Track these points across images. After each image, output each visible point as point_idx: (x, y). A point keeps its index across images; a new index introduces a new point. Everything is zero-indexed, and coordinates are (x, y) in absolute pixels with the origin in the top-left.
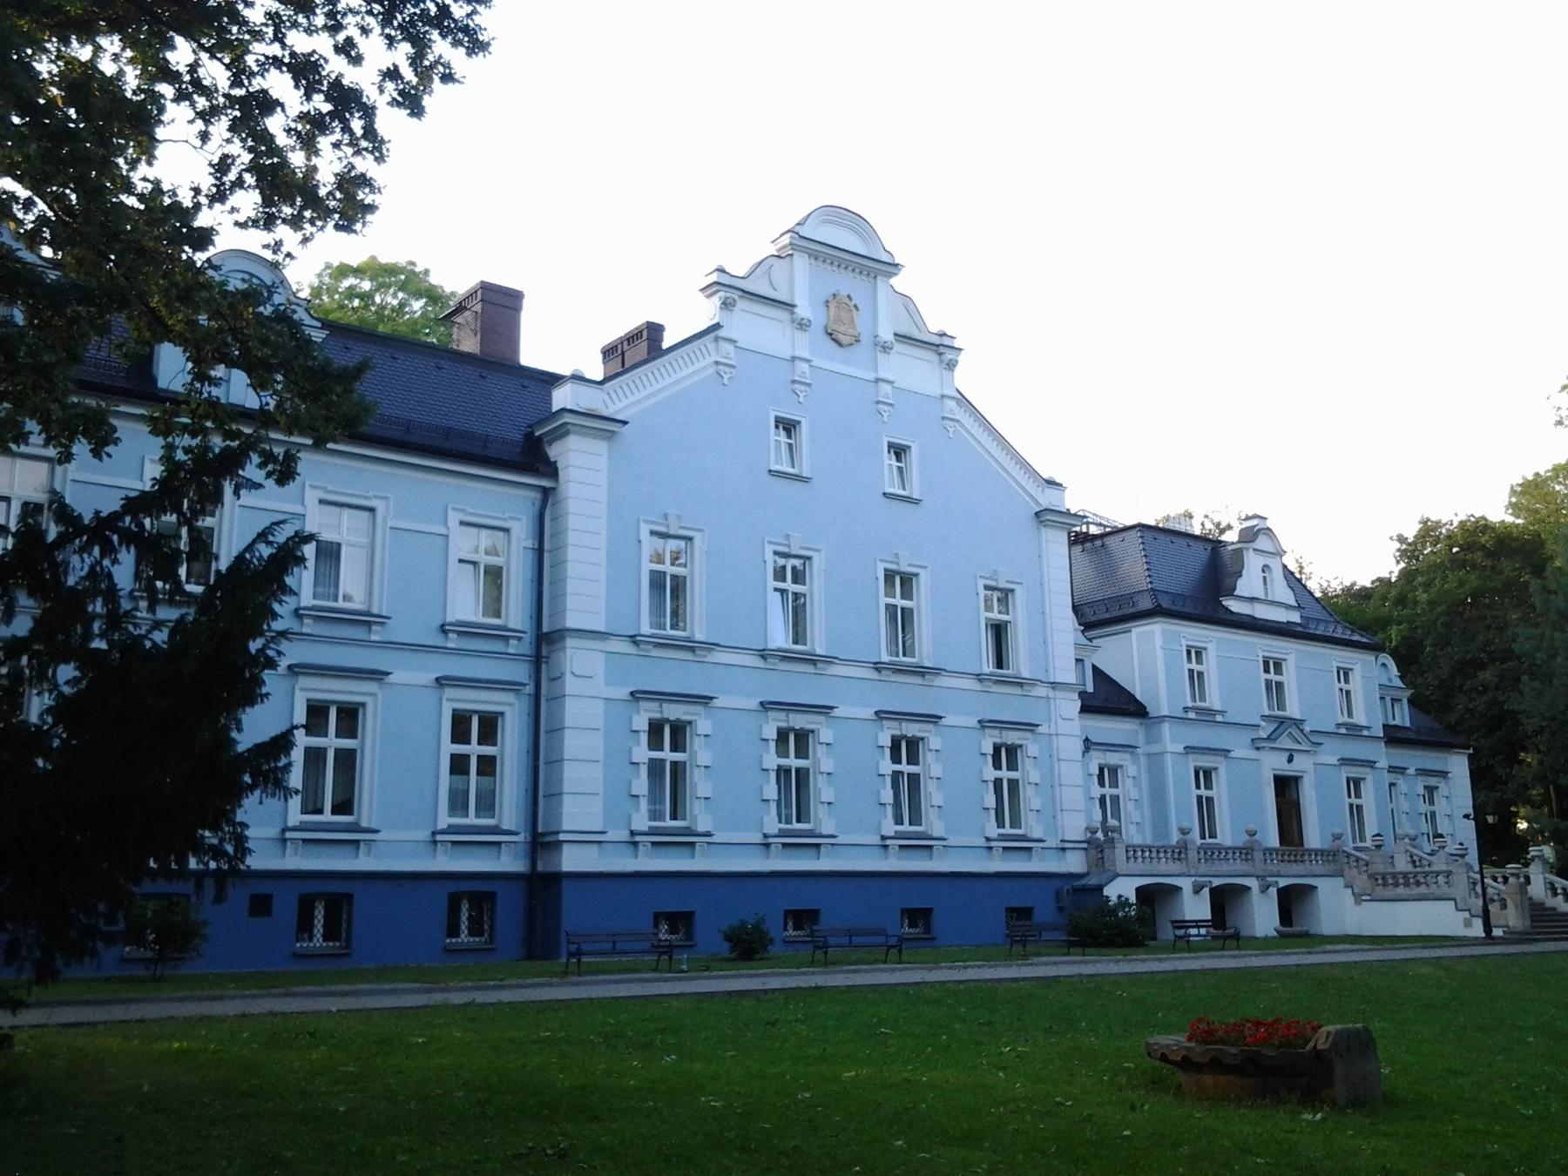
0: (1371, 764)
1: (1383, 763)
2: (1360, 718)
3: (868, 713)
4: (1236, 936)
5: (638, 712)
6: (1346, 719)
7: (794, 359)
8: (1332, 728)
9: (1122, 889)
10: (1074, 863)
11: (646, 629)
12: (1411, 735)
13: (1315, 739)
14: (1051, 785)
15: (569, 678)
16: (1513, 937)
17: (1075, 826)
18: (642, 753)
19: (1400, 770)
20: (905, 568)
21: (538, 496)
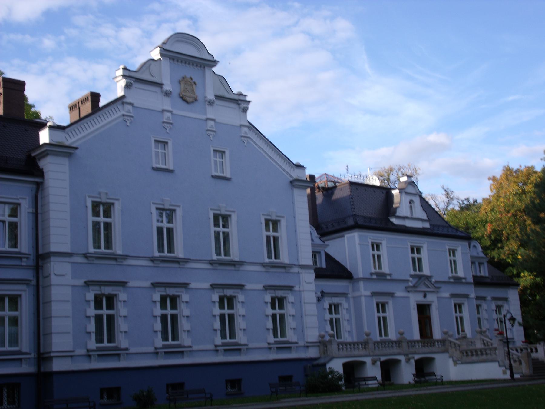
0: (466, 296)
1: (473, 295)
2: (461, 274)
3: (207, 285)
4: (392, 384)
5: (89, 292)
6: (378, 270)
7: (163, 111)
8: (446, 279)
9: (336, 366)
10: (312, 353)
11: (91, 250)
12: (489, 281)
13: (437, 286)
14: (300, 316)
15: (53, 277)
16: (524, 378)
17: (312, 335)
18: (92, 311)
19: (484, 298)
20: (223, 212)
21: (34, 186)
